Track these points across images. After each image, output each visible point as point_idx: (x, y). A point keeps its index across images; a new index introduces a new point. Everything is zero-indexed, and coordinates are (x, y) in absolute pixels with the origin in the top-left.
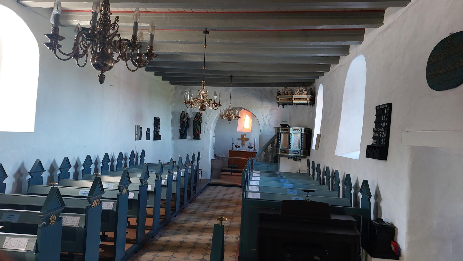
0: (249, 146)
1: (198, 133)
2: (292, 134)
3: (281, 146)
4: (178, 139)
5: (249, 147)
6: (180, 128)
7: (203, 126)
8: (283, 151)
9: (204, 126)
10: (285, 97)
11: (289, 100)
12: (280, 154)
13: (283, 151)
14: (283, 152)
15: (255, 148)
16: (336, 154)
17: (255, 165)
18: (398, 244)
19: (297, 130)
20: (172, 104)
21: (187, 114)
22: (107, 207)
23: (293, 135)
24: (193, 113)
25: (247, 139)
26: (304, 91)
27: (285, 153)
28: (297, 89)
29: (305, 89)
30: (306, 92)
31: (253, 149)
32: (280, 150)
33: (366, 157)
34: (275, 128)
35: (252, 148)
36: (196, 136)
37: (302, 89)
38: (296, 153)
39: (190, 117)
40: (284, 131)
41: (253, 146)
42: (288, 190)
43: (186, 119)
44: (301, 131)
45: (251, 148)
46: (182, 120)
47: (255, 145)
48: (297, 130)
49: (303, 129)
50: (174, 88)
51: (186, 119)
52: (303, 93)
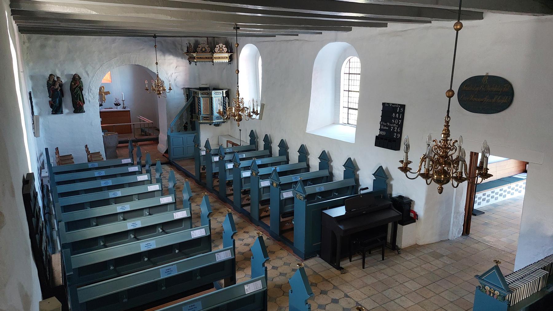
0: (115, 103)
1: (81, 104)
2: (214, 98)
3: (202, 112)
4: (49, 114)
5: (116, 105)
6: (50, 99)
7: (86, 93)
8: (205, 118)
9: (87, 94)
10: (203, 55)
11: (209, 58)
12: (201, 121)
13: (204, 118)
14: (205, 119)
15: (123, 104)
16: (307, 131)
17: (173, 137)
18: (415, 212)
19: (218, 93)
20: (28, 64)
21: (58, 78)
22: (225, 256)
23: (214, 99)
24: (67, 76)
25: (107, 93)
26: (224, 49)
27: (208, 120)
28: (217, 46)
29: (225, 46)
30: (227, 49)
31: (122, 105)
32: (201, 117)
33: (376, 145)
34: (183, 88)
35: (120, 105)
36: (78, 108)
37: (222, 46)
38: (219, 119)
39: (63, 81)
40: (204, 95)
41: (121, 103)
42: (293, 178)
43: (57, 86)
44: (223, 94)
45: (119, 105)
46: (53, 87)
47: (123, 101)
48: (218, 93)
49: (224, 91)
50: (26, 39)
51: (58, 85)
52: (224, 50)
